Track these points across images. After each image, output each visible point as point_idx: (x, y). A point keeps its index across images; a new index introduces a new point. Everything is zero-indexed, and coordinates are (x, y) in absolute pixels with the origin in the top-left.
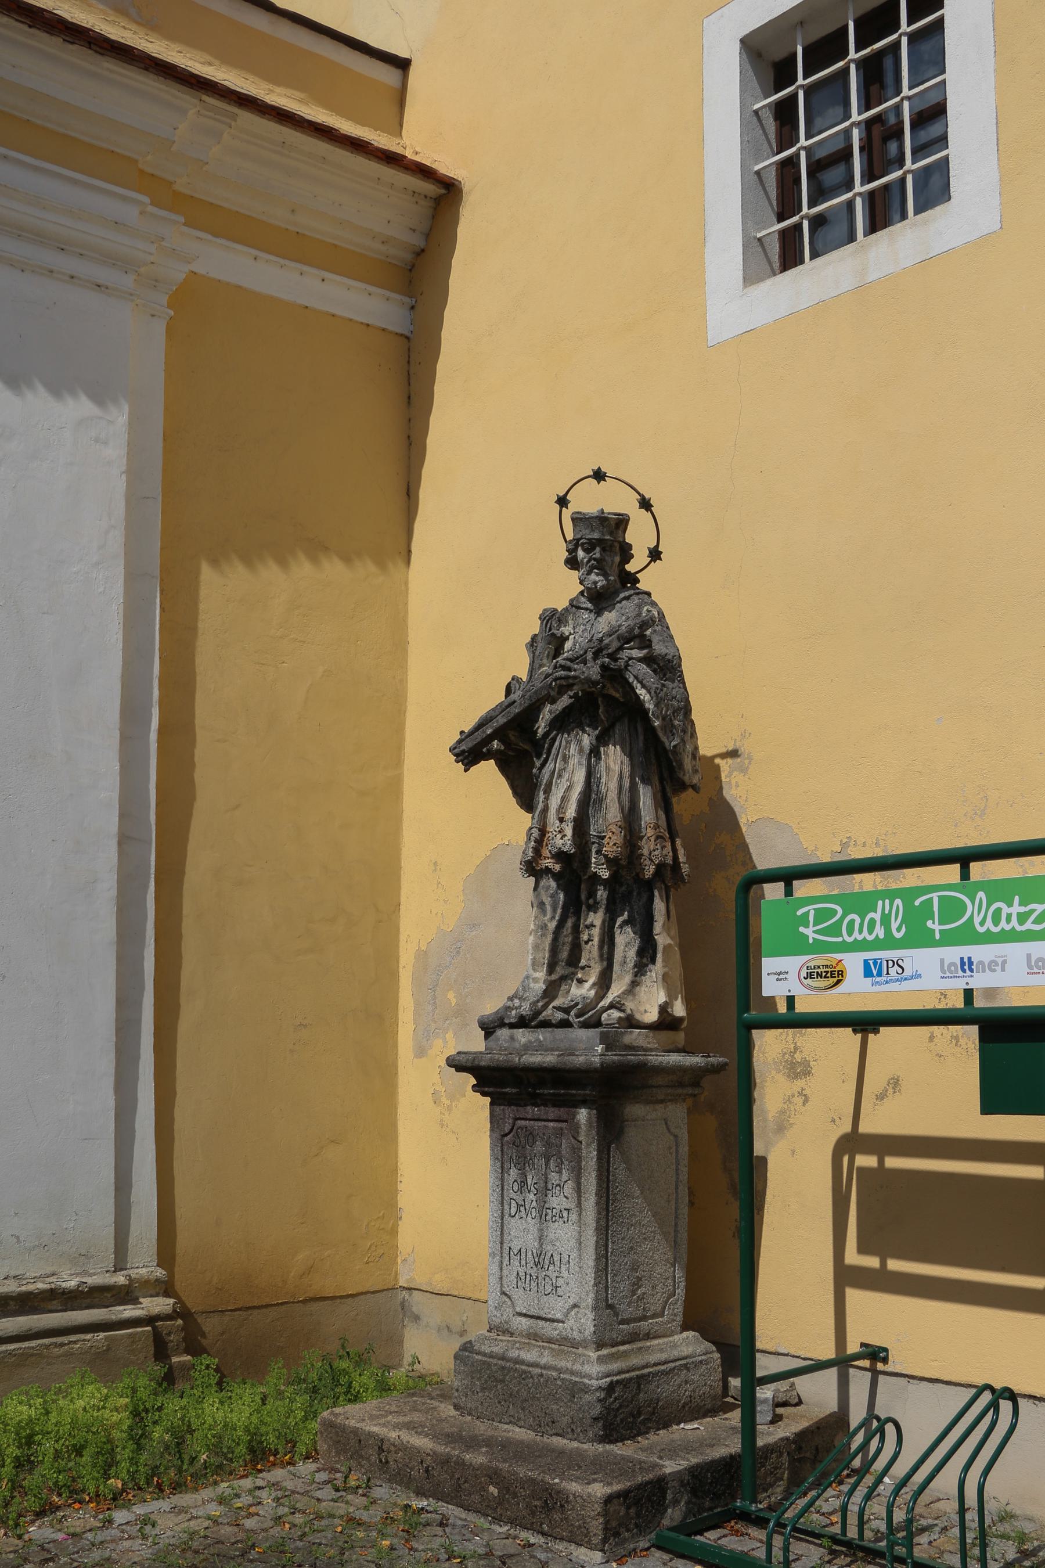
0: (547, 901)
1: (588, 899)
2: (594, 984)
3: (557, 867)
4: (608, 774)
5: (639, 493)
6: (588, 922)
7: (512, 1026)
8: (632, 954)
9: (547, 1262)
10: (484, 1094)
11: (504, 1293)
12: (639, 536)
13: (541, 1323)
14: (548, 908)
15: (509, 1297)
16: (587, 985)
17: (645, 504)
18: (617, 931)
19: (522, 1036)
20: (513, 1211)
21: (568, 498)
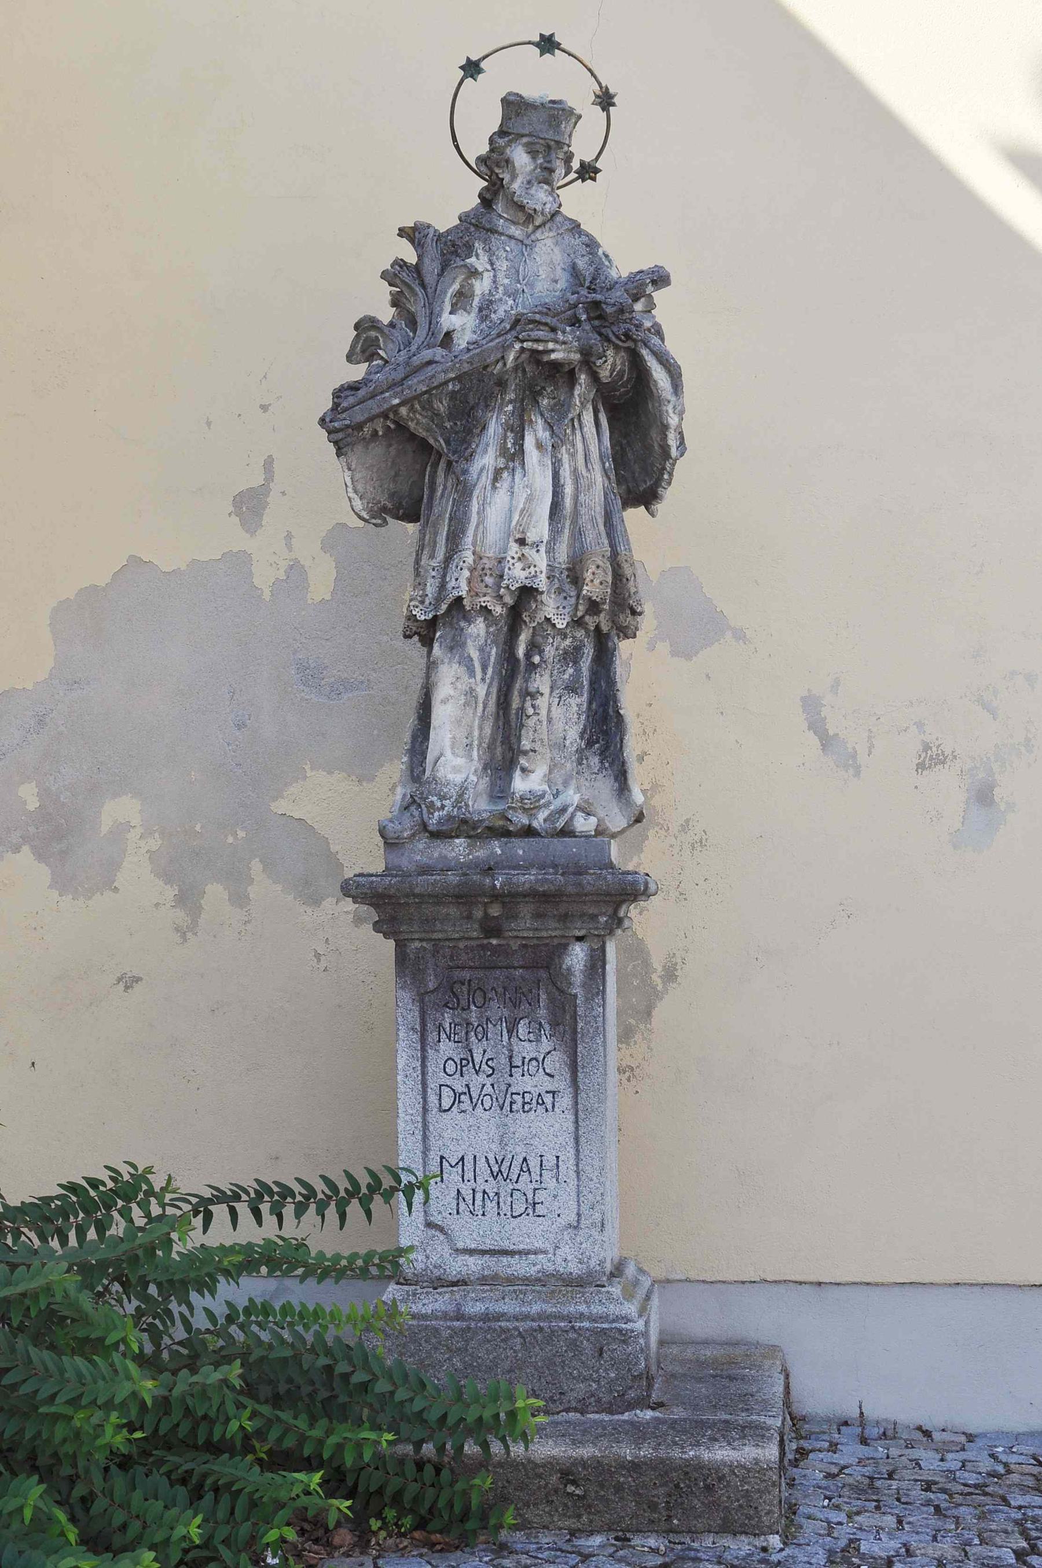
5: (600, 84)
9: (515, 1170)
10: (386, 936)
11: (429, 1225)
13: (505, 1260)
15: (441, 1229)
17: (605, 100)
20: (446, 1103)
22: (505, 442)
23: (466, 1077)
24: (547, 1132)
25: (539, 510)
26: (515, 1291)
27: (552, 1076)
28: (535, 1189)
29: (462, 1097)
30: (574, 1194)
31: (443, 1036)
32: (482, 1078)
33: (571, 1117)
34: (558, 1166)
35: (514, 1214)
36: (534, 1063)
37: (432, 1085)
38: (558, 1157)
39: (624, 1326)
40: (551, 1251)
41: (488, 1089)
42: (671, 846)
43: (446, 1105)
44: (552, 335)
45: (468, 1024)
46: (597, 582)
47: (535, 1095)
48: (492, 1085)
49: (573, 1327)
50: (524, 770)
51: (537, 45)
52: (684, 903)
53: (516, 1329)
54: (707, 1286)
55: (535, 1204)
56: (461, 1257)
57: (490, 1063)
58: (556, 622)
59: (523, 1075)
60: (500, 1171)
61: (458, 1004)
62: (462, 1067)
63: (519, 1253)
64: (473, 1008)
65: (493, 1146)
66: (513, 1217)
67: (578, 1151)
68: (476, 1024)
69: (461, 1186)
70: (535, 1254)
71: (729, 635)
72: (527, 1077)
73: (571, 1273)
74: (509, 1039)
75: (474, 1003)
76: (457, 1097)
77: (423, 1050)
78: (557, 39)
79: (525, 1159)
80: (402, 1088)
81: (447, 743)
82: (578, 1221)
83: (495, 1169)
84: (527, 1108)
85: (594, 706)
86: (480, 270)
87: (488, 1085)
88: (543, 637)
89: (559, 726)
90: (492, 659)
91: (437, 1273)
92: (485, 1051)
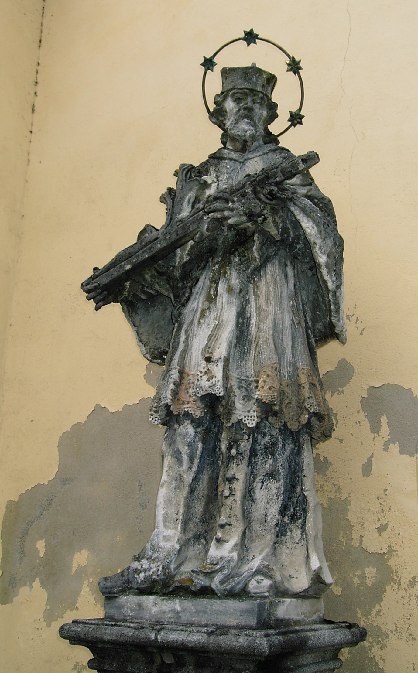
0: (185, 450)
1: (229, 449)
2: (236, 545)
3: (198, 413)
4: (258, 315)
5: (288, 56)
6: (229, 474)
7: (142, 592)
8: (274, 511)
12: (284, 96)
14: (185, 458)
16: (228, 546)
17: (294, 67)
18: (257, 485)
19: (154, 606)
21: (214, 60)
22: (210, 291)
25: (223, 335)
42: (403, 597)
44: (226, 205)
46: (266, 388)
50: (218, 541)
51: (244, 39)
52: (412, 642)
58: (247, 422)
78: (255, 32)
86: (209, 182)
88: (241, 435)
90: (199, 452)
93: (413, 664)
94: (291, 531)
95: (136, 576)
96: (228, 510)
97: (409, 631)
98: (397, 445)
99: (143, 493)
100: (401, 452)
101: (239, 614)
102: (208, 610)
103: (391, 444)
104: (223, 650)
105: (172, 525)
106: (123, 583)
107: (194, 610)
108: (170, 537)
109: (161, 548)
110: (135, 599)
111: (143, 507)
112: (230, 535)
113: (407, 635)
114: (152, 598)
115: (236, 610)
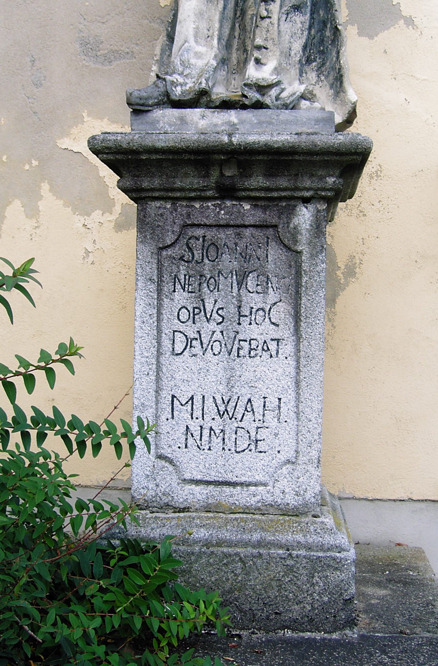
11: (160, 457)
13: (227, 490)
15: (171, 462)
20: (179, 348)
23: (198, 325)
24: (269, 376)
26: (236, 519)
27: (278, 326)
28: (258, 428)
29: (194, 342)
30: (293, 433)
31: (178, 286)
32: (212, 326)
33: (293, 363)
34: (279, 408)
35: (238, 450)
36: (261, 313)
37: (167, 331)
38: (280, 399)
39: (338, 555)
40: (271, 483)
41: (218, 336)
43: (178, 349)
45: (201, 276)
47: (261, 342)
48: (222, 332)
49: (290, 555)
52: (363, 218)
53: (237, 554)
54: (368, 503)
55: (257, 441)
56: (188, 487)
57: (220, 312)
59: (250, 324)
60: (226, 410)
61: (193, 258)
62: (194, 315)
63: (242, 484)
64: (206, 261)
65: (221, 388)
66: (237, 452)
67: (298, 394)
68: (209, 276)
69: (190, 423)
70: (256, 485)
71: (402, 22)
72: (254, 326)
73: (288, 504)
74: (239, 290)
75: (208, 257)
76: (189, 343)
77: (159, 299)
79: (249, 400)
80: (139, 333)
81: (191, 32)
82: (296, 458)
83: (222, 408)
84: (253, 353)
85: (313, 32)
87: (218, 333)
89: (286, 37)
91: (165, 500)
92: (216, 301)
93: (363, 239)
94: (306, 73)
95: (174, 89)
96: (264, 32)
97: (359, 208)
98: (356, 27)
99: (38, 70)
100: (360, 34)
101: (313, 123)
102: (274, 121)
103: (349, 26)
104: (318, 149)
105: (203, 42)
106: (160, 95)
107: (255, 122)
108: (202, 54)
109: (192, 65)
110: (175, 113)
111: (38, 85)
112: (267, 59)
113: (358, 212)
114: (198, 111)
115: (309, 119)
